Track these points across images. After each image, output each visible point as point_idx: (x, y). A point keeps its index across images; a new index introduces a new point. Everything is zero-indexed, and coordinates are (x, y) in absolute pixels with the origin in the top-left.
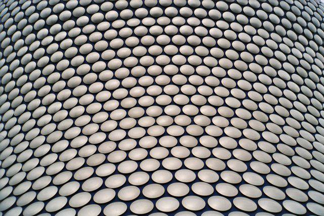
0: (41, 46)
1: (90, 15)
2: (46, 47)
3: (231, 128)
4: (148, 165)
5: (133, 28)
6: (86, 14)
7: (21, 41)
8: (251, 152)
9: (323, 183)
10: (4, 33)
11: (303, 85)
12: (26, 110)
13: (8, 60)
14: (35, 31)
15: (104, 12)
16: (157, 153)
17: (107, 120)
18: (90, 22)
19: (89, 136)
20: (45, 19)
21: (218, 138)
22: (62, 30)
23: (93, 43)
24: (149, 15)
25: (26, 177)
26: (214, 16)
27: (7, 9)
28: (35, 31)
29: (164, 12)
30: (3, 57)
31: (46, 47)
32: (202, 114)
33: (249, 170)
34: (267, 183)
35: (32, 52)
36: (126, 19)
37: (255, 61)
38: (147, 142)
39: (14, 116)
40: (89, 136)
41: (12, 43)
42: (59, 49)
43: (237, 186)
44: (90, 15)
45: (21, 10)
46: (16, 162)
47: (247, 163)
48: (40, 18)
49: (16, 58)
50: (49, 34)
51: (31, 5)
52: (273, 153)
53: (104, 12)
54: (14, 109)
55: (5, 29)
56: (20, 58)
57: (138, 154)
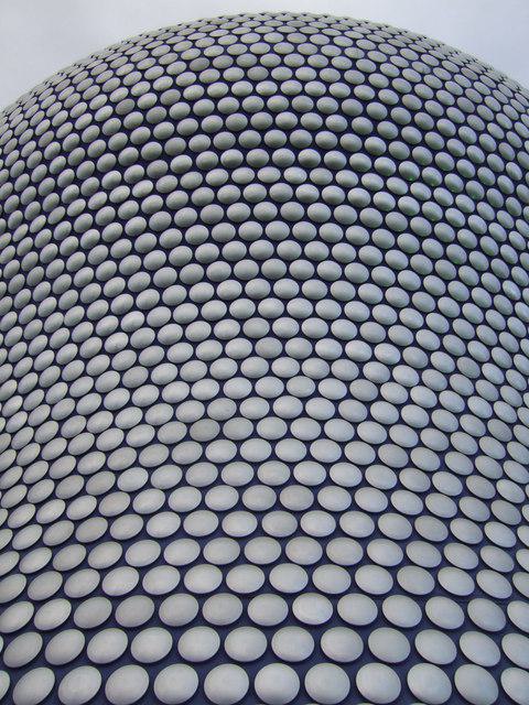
0: (108, 203)
1: (193, 154)
2: (117, 205)
3: (421, 388)
4: (288, 450)
5: (268, 185)
6: (187, 151)
7: (73, 189)
8: (448, 434)
9: (527, 670)
10: (8, 186)
11: (519, 301)
12: (85, 319)
13: (51, 219)
14: (98, 174)
15: (219, 152)
16: (302, 428)
17: (170, 421)
18: (194, 168)
19: (191, 384)
20: (117, 153)
21: (399, 407)
22: (145, 177)
23: (199, 208)
24: (297, 164)
25: (94, 445)
26: (382, 205)
27: (47, 122)
28: (98, 174)
29: (322, 159)
30: (7, 230)
31: (117, 205)
32: (328, 438)
33: (444, 467)
34: (467, 492)
35: (94, 212)
36: (256, 167)
37: (437, 310)
38: (285, 406)
39: (63, 326)
40: (191, 384)
41: (58, 190)
42: (140, 213)
43: (422, 495)
44: (193, 154)
45: (74, 130)
46: (74, 413)
47: (441, 454)
48: (107, 150)
49: (66, 218)
50: (123, 182)
51: (112, 117)
52: (468, 476)
53: (219, 152)
54: (64, 312)
55: (11, 180)
56: (72, 219)
57: (270, 428)
